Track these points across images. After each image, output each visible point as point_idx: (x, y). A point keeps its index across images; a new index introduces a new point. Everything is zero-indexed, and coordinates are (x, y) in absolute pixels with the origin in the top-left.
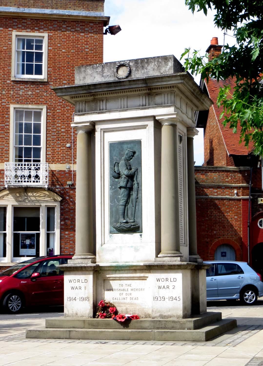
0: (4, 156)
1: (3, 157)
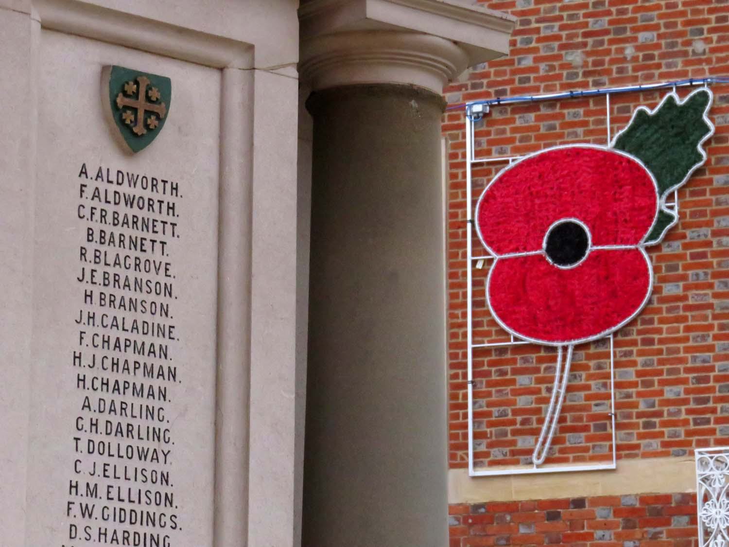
0: (713, 411)
1: (708, 421)
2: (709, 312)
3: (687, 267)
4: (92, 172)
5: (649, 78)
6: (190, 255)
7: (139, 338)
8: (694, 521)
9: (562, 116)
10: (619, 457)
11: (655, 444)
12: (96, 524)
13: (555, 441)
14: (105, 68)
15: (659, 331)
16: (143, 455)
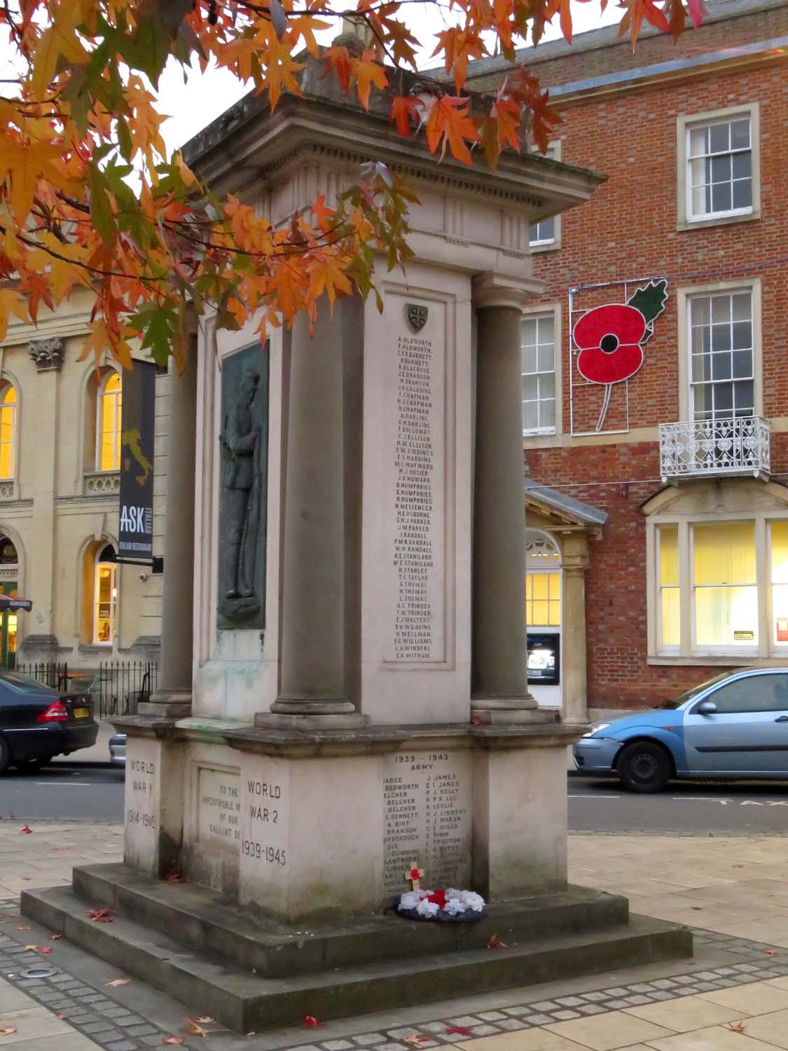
2: (665, 370)
3: (657, 352)
4: (402, 339)
5: (642, 276)
6: (435, 365)
7: (419, 394)
8: (659, 452)
9: (607, 293)
10: (630, 428)
11: (644, 423)
12: (406, 454)
13: (604, 422)
14: (406, 305)
15: (646, 378)
16: (421, 432)
